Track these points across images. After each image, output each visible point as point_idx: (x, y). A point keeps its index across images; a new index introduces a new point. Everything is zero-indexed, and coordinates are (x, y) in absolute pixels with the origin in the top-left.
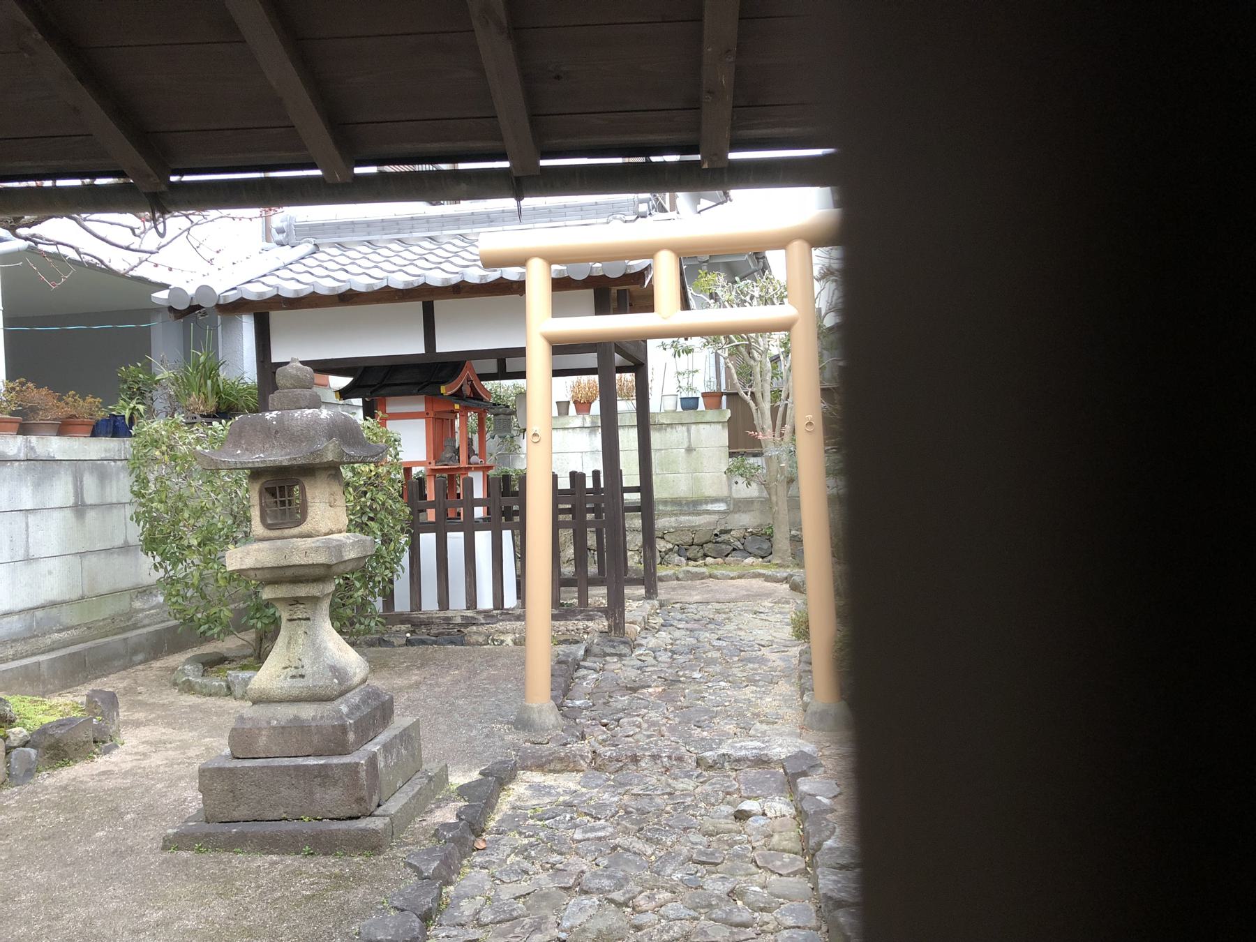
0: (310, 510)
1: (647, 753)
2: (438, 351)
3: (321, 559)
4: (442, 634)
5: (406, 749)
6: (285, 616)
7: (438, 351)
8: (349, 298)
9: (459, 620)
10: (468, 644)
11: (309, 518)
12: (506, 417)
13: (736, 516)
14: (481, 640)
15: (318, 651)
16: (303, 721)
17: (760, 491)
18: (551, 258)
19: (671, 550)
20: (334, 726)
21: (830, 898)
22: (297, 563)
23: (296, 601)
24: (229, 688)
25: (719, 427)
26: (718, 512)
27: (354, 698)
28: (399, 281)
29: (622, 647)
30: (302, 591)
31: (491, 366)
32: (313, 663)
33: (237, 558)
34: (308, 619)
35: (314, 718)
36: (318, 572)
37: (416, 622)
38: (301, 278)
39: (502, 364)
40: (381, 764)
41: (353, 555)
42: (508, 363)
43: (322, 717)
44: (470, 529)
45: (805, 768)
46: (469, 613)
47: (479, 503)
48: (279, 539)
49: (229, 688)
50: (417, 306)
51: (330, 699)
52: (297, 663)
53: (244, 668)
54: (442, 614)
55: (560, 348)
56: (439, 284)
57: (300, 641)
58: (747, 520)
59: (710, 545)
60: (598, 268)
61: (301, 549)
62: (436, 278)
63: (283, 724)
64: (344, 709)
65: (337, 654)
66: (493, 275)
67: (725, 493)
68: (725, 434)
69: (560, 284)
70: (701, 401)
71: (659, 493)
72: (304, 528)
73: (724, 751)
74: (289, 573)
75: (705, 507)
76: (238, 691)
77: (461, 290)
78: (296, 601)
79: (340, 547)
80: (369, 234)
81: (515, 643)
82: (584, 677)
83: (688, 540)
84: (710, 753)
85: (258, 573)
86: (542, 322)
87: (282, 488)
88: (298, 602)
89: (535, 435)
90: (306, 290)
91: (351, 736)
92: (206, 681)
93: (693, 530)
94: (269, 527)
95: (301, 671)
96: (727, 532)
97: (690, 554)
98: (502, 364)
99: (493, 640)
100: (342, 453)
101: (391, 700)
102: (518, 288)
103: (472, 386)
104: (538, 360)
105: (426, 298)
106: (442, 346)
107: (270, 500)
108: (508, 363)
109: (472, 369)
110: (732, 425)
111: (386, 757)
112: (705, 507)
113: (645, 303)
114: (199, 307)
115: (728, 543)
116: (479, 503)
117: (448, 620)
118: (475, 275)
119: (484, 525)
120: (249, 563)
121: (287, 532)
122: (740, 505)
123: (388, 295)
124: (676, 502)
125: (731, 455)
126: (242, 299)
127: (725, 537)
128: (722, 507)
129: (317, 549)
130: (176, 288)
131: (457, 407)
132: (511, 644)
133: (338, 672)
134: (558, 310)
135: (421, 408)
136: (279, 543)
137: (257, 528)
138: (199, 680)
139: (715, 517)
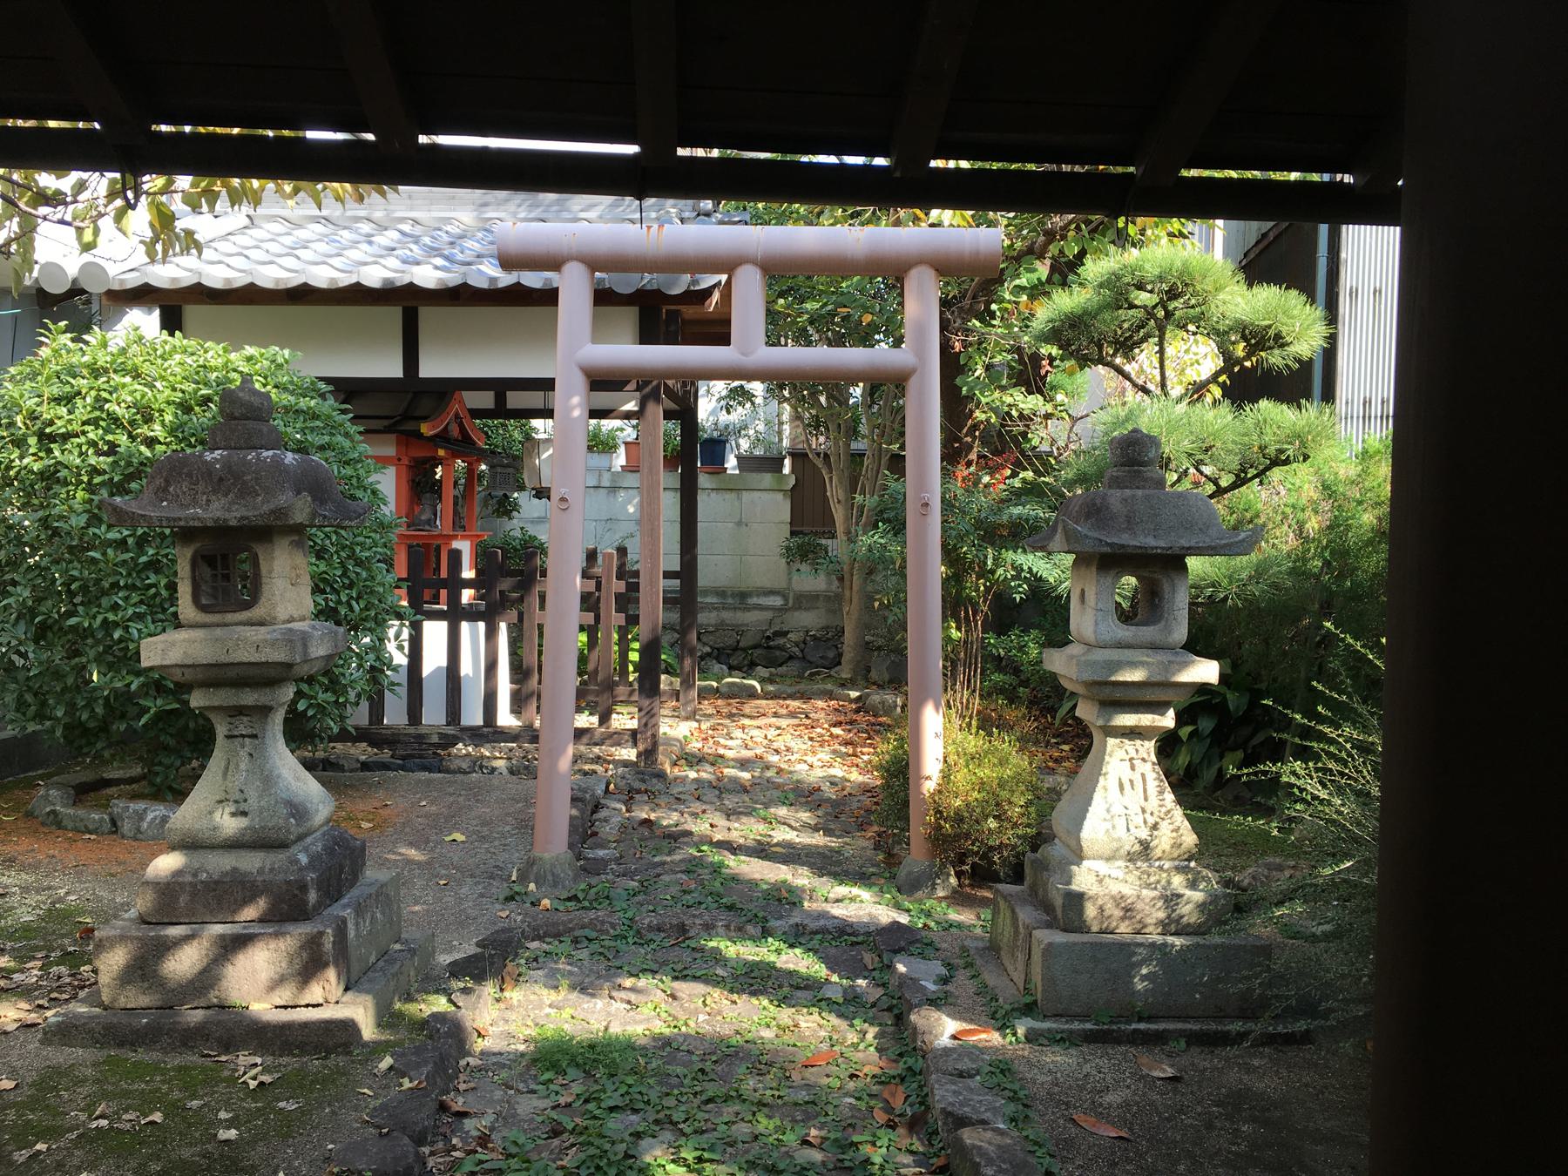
0: (265, 588)
1: (698, 921)
2: (421, 375)
3: (278, 656)
4: (412, 756)
5: (383, 913)
6: (221, 730)
7: (421, 375)
8: (303, 295)
9: (435, 739)
10: (448, 771)
11: (263, 600)
12: (511, 467)
13: (796, 614)
14: (464, 766)
15: (268, 780)
16: (245, 874)
17: (830, 583)
18: (594, 263)
19: (709, 655)
20: (288, 883)
21: (950, 1114)
22: (245, 660)
23: (238, 711)
24: (114, 822)
25: (780, 496)
26: (773, 608)
27: (316, 844)
28: (373, 277)
29: (654, 781)
30: (249, 698)
31: (486, 400)
32: (261, 797)
33: (162, 650)
34: (254, 736)
35: (261, 871)
36: (273, 673)
37: (373, 735)
38: (233, 261)
39: (500, 399)
40: (351, 933)
41: (322, 652)
42: (517, 399)
43: (272, 870)
44: (455, 615)
45: (903, 944)
46: (450, 730)
47: (468, 584)
48: (218, 625)
49: (114, 822)
50: (394, 314)
51: (283, 845)
52: (237, 796)
53: (135, 797)
54: (412, 730)
55: (602, 381)
56: (323, 285)
57: (243, 766)
58: (809, 620)
59: (759, 651)
60: (647, 280)
61: (247, 642)
62: (428, 276)
63: (215, 877)
64: (304, 859)
65: (294, 785)
66: (506, 279)
67: (781, 584)
68: (786, 507)
69: (603, 297)
70: (787, 462)
71: (703, 580)
72: (256, 612)
73: (798, 920)
74: (232, 673)
75: (754, 600)
76: (126, 827)
77: (459, 295)
78: (238, 711)
79: (305, 638)
80: (411, 210)
81: (512, 772)
82: (606, 820)
83: (731, 642)
84: (779, 923)
85: (187, 671)
86: (579, 342)
87: (225, 557)
88: (241, 714)
89: (563, 499)
90: (240, 280)
91: (312, 896)
92: (81, 812)
93: (739, 630)
94: (203, 609)
95: (243, 807)
96: (785, 634)
97: (733, 662)
98: (500, 399)
99: (481, 767)
100: (314, 515)
101: (363, 848)
102: (549, 297)
103: (461, 426)
104: (572, 400)
105: (407, 302)
106: (430, 368)
107: (206, 571)
108: (517, 399)
109: (462, 402)
110: (796, 494)
111: (357, 924)
112: (754, 600)
113: (717, 331)
114: (83, 292)
115: (781, 648)
116: (468, 584)
117: (420, 738)
118: (489, 273)
119: (472, 615)
120: (174, 657)
121: (230, 617)
122: (804, 601)
123: (356, 295)
124: (721, 593)
125: (793, 533)
126: (147, 285)
127: (781, 641)
128: (777, 601)
129: (273, 644)
130: (48, 264)
131: (441, 453)
132: (505, 772)
133: (298, 811)
134: (599, 333)
135: (390, 451)
136: (218, 631)
137: (185, 607)
138: (71, 811)
139: (768, 615)
